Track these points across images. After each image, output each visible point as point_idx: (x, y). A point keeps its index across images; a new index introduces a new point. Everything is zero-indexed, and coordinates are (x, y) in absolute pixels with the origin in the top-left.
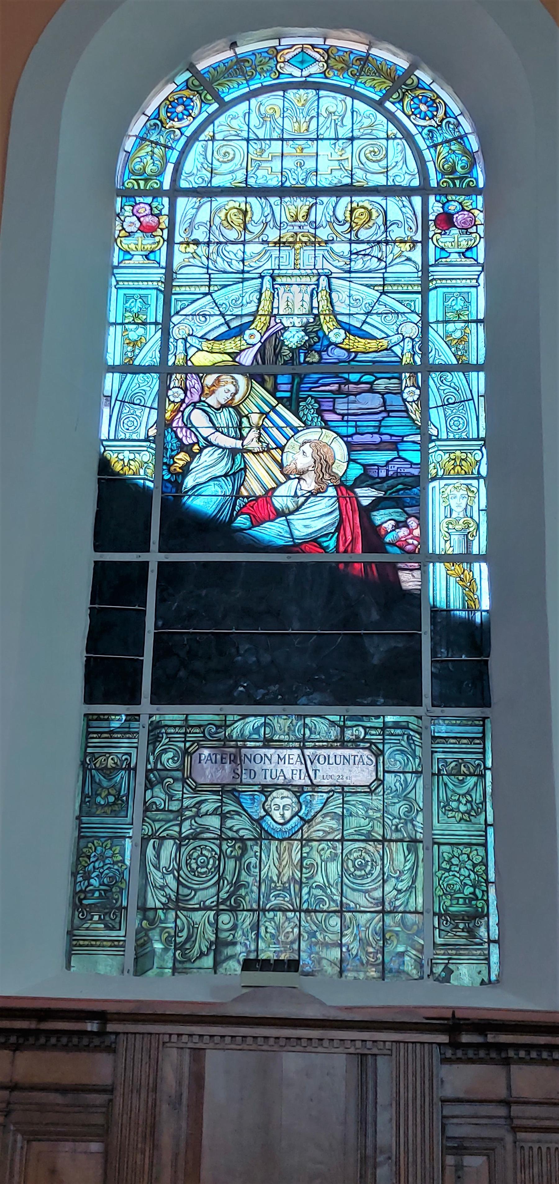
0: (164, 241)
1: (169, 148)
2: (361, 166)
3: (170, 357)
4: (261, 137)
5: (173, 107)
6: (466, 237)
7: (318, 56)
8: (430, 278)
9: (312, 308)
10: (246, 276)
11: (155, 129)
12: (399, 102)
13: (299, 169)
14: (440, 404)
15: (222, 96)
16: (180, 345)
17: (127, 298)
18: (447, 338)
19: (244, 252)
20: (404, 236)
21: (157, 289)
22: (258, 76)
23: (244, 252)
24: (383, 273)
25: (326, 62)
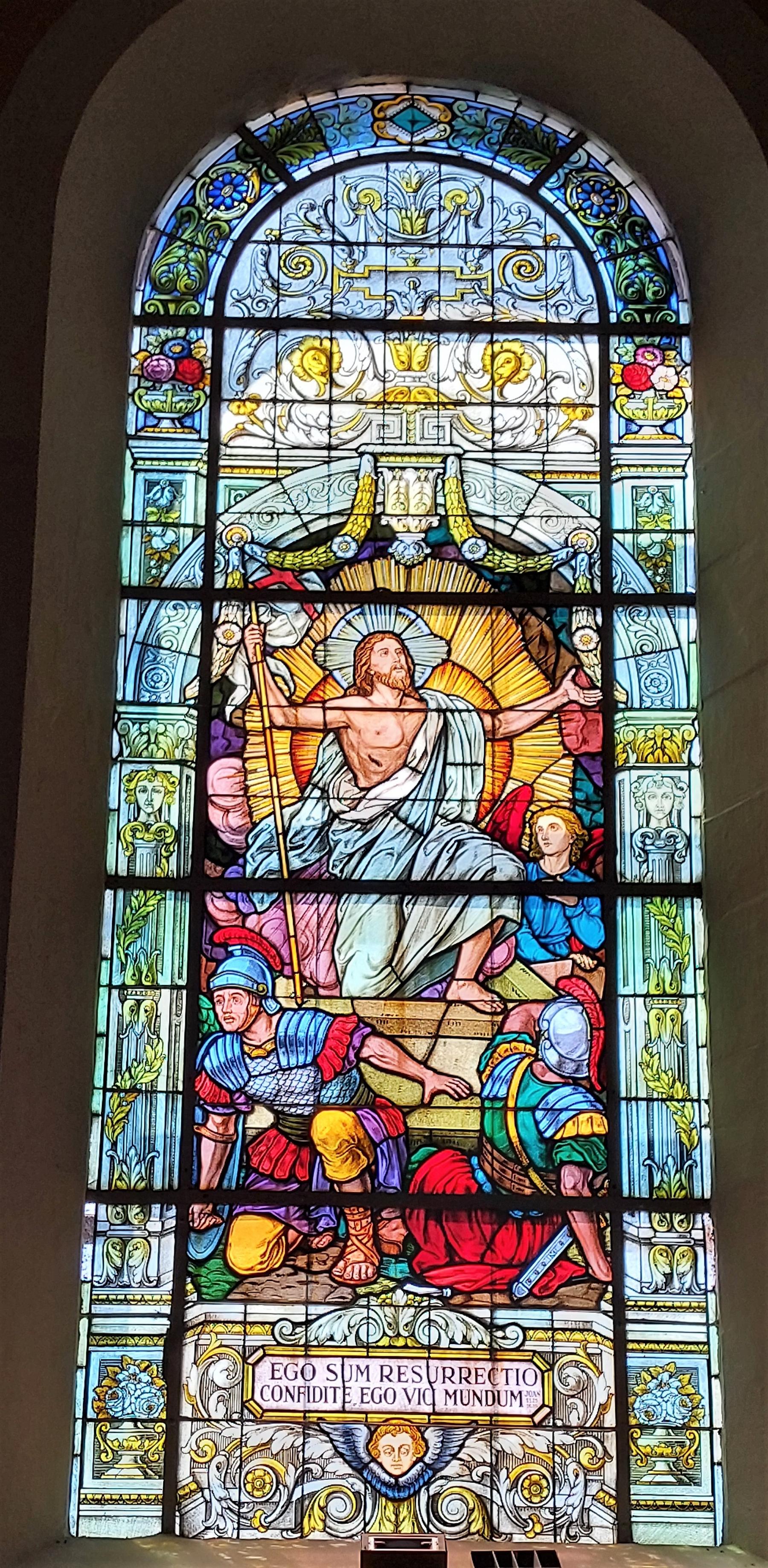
0: (207, 397)
1: (214, 252)
2: (506, 288)
3: (217, 576)
4: (352, 239)
5: (215, 188)
6: (667, 403)
7: (435, 114)
8: (614, 463)
9: (436, 505)
10: (334, 453)
11: (189, 221)
12: (558, 188)
13: (413, 292)
14: (631, 654)
15: (290, 170)
16: (234, 558)
17: (150, 485)
18: (639, 554)
19: (330, 417)
20: (574, 396)
21: (197, 473)
22: (344, 141)
23: (330, 417)
24: (544, 453)
25: (449, 123)
